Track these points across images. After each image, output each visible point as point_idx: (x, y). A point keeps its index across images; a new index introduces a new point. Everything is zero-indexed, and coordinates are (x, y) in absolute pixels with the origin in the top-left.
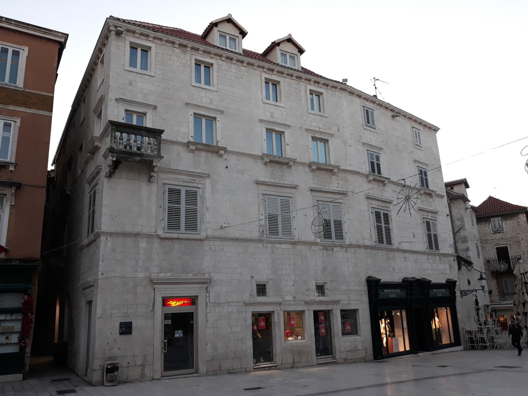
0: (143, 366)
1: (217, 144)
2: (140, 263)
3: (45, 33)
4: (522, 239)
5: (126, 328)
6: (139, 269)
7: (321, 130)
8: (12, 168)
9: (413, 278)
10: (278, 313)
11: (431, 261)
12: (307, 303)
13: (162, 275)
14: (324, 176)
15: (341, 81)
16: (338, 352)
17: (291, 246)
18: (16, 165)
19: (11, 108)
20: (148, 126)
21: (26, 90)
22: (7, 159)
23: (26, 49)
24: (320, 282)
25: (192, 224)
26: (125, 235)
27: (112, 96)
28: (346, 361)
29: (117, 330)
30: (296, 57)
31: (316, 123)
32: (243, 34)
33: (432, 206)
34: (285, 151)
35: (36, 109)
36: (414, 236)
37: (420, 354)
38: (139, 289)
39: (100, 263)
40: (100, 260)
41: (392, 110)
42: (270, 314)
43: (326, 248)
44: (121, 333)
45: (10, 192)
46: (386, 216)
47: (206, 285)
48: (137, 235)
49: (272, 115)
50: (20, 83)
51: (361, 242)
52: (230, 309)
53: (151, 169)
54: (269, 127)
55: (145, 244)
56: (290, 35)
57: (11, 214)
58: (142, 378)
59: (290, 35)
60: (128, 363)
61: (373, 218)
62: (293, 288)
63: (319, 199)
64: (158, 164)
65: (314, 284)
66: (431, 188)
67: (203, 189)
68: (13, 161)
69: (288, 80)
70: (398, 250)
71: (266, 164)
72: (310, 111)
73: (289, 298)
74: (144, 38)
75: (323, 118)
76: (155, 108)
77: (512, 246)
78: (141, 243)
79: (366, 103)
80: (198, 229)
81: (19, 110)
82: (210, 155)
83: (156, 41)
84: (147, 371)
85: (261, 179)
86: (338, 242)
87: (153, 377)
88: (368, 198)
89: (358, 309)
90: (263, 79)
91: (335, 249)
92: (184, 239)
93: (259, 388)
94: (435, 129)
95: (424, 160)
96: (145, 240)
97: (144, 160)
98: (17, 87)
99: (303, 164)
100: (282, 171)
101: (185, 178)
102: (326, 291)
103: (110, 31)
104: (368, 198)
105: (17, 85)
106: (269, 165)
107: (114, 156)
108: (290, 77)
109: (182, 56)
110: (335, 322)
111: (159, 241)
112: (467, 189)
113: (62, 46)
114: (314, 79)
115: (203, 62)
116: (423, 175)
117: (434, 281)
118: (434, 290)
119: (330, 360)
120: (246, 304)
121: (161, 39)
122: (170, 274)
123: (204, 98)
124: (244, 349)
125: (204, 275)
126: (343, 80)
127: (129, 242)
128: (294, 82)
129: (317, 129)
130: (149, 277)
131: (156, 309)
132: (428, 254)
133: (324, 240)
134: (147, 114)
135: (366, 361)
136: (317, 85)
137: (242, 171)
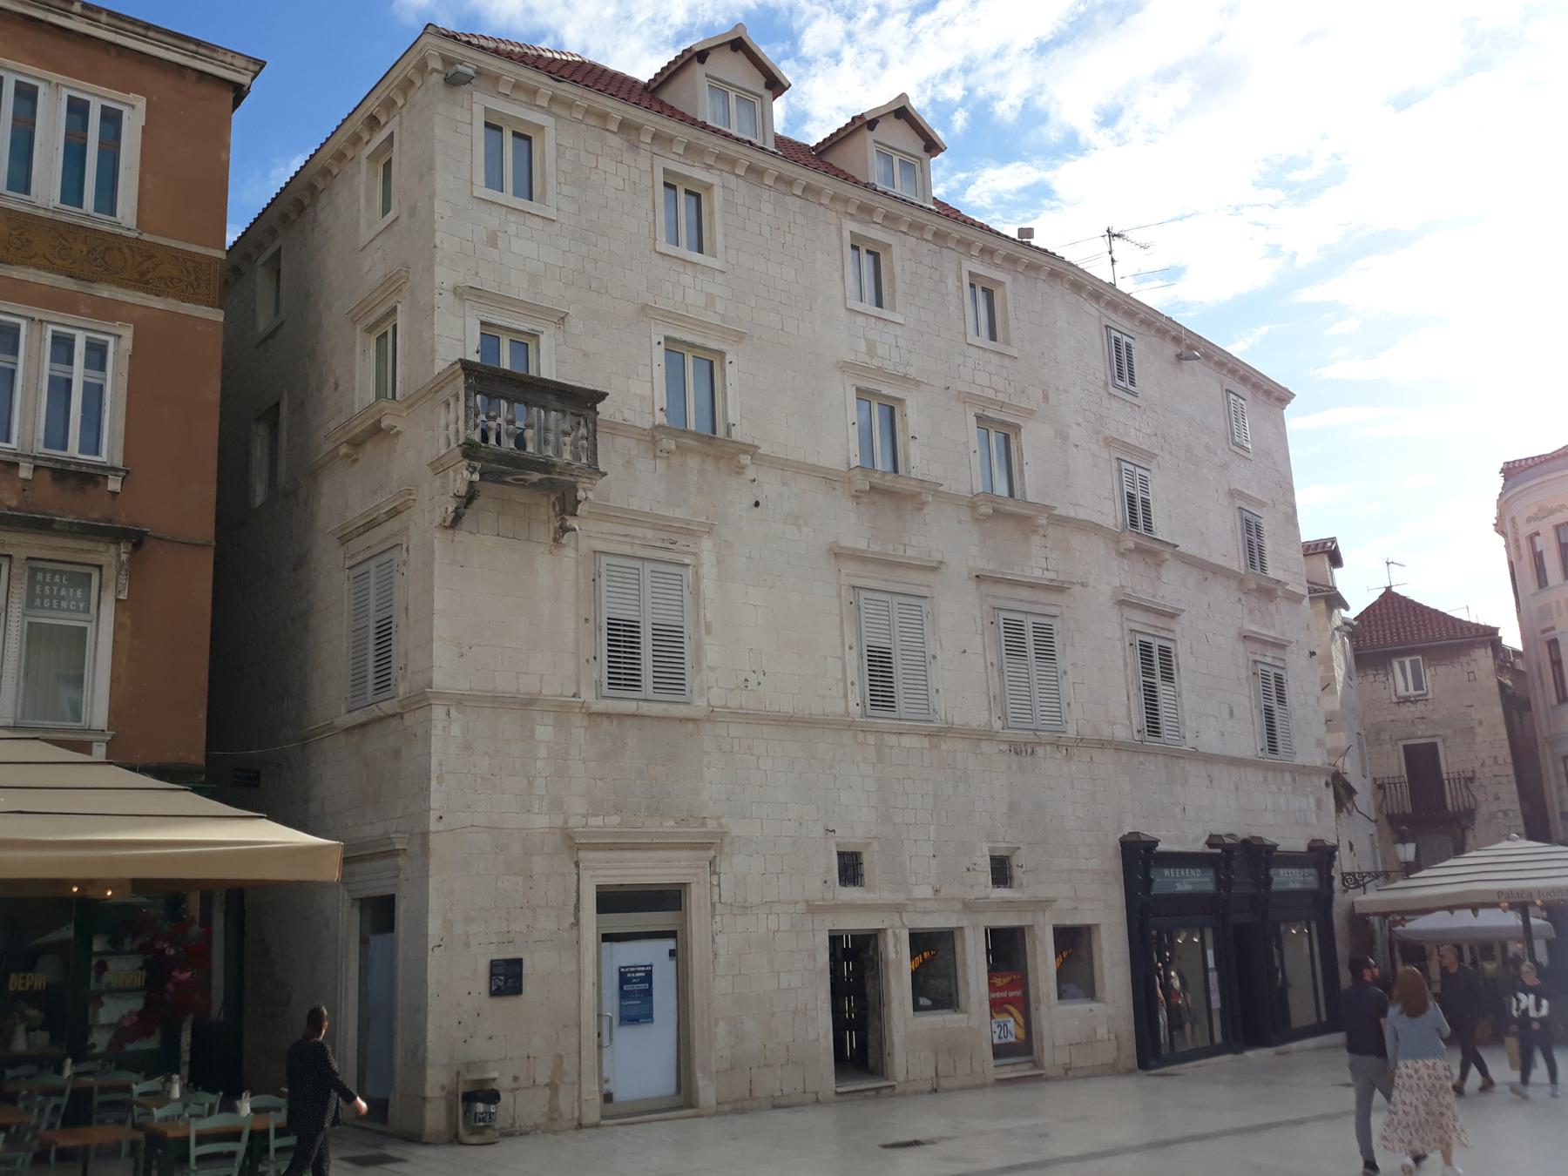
0: (553, 1086)
1: (728, 433)
2: (540, 783)
3: (194, 55)
4: (1480, 723)
5: (507, 978)
7: (1001, 397)
8: (114, 484)
9: (1230, 835)
10: (895, 935)
12: (968, 907)
13: (595, 821)
15: (1015, 235)
16: (1047, 1045)
17: (926, 742)
19: (106, 294)
20: (545, 375)
21: (146, 237)
22: (97, 453)
23: (141, 103)
24: (1002, 848)
26: (498, 702)
27: (444, 276)
28: (1068, 1073)
29: (482, 983)
30: (917, 166)
32: (776, 86)
34: (907, 459)
35: (175, 297)
37: (1250, 1054)
39: (433, 783)
40: (434, 776)
41: (1177, 340)
44: (496, 992)
45: (111, 556)
46: (1165, 652)
47: (712, 853)
48: (526, 704)
49: (871, 348)
51: (1106, 732)
53: (569, 509)
54: (864, 384)
55: (550, 729)
56: (903, 96)
57: (118, 627)
58: (551, 1125)
59: (903, 96)
60: (516, 1079)
61: (1135, 659)
62: (933, 862)
63: (857, 582)
64: (590, 495)
67: (697, 567)
68: (118, 463)
70: (1195, 755)
71: (979, 520)
72: (663, 246)
75: (1007, 362)
81: (128, 299)
83: (556, 109)
84: (565, 1102)
85: (847, 542)
87: (580, 1118)
88: (1122, 603)
89: (1097, 925)
90: (847, 235)
91: (1040, 751)
92: (651, 717)
93: (916, 1143)
94: (1282, 397)
98: (119, 225)
99: (954, 499)
101: (650, 534)
102: (1017, 873)
103: (422, 68)
105: (119, 218)
108: (917, 234)
110: (1039, 959)
112: (1336, 571)
113: (239, 93)
114: (981, 240)
116: (1252, 531)
118: (1166, 872)
119: (1025, 1070)
120: (813, 909)
121: (570, 105)
122: (616, 819)
123: (695, 293)
125: (704, 825)
126: (1021, 231)
129: (989, 393)
130: (563, 829)
131: (583, 920)
132: (1267, 768)
133: (869, 712)
134: (542, 338)
136: (987, 258)
137: (797, 518)
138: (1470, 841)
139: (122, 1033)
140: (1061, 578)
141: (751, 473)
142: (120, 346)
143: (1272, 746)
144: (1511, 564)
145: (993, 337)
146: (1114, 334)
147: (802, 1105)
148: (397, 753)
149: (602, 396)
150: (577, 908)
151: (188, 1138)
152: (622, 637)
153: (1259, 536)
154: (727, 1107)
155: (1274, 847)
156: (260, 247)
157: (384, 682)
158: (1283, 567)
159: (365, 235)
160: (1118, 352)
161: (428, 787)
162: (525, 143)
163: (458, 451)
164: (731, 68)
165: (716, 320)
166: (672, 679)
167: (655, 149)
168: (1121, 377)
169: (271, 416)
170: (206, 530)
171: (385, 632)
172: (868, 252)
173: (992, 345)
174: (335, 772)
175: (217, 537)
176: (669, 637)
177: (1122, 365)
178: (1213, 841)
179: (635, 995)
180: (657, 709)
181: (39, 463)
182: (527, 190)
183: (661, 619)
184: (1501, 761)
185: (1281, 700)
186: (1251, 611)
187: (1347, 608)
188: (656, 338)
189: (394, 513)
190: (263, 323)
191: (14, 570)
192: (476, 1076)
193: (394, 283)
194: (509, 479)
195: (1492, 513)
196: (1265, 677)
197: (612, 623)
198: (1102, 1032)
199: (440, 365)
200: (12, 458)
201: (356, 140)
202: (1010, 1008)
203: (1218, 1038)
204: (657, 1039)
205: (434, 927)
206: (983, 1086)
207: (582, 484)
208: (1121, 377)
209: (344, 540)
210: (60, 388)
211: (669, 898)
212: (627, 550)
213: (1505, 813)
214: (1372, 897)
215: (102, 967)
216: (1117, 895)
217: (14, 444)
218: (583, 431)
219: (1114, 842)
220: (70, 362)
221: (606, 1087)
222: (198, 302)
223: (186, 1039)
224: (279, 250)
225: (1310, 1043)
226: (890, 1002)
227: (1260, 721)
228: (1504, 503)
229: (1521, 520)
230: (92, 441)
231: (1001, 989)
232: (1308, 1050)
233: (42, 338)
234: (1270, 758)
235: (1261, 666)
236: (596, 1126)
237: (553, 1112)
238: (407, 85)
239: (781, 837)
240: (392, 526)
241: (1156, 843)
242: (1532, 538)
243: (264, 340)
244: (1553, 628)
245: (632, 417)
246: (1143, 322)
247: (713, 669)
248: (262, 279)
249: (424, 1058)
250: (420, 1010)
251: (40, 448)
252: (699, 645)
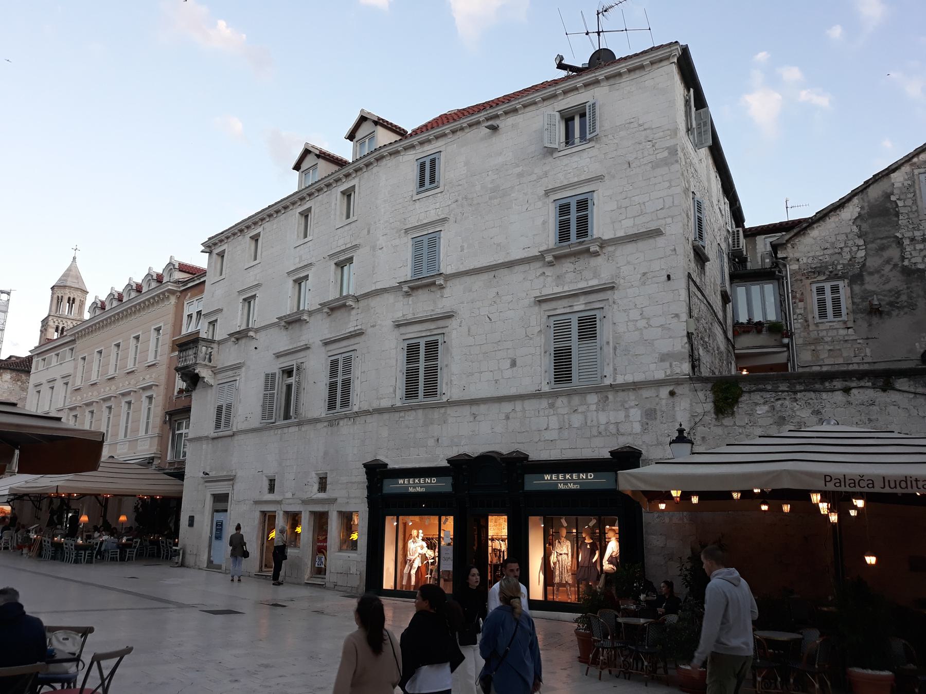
12: (305, 502)
14: (423, 295)
17: (296, 429)
25: (432, 389)
28: (335, 587)
54: (294, 278)
61: (402, 356)
70: (451, 404)
73: (289, 495)
88: (398, 326)
117: (537, 454)
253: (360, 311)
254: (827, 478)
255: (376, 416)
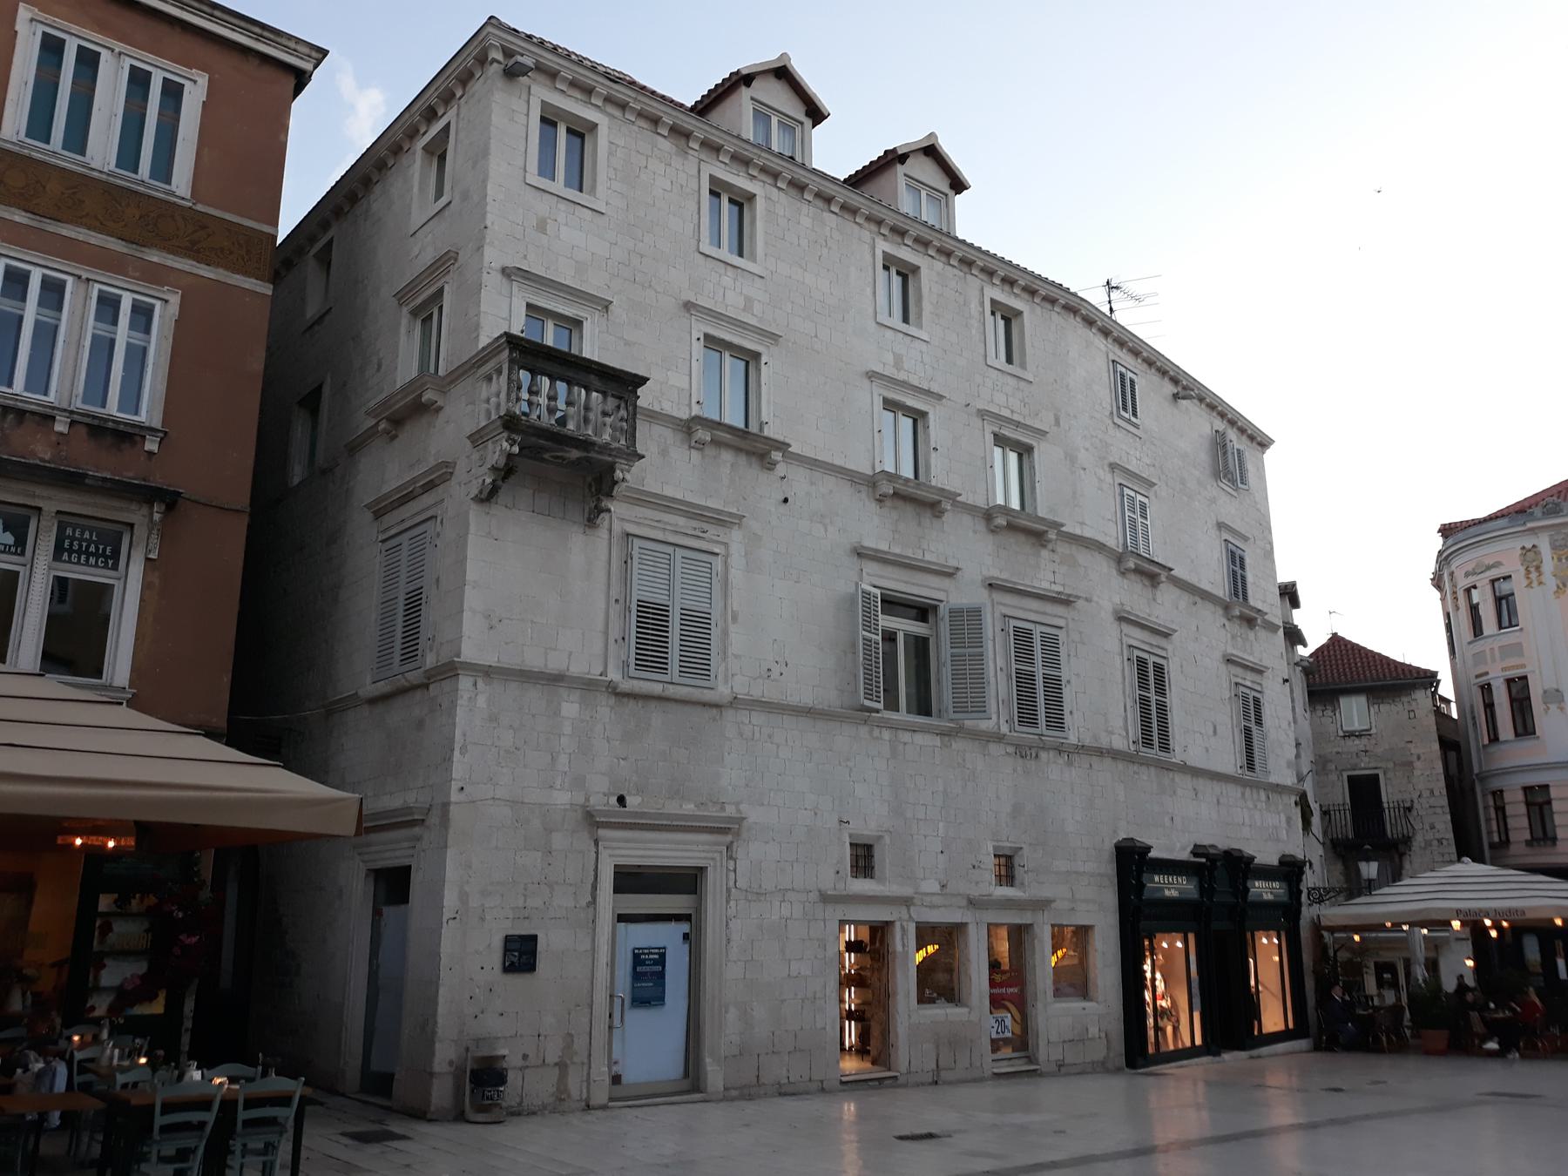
0: (562, 1066)
1: (761, 429)
2: (563, 759)
5: (521, 954)
6: (558, 782)
7: (1016, 417)
8: (151, 445)
9: (1212, 846)
11: (1250, 804)
12: (973, 903)
14: (1019, 546)
16: (1042, 1043)
17: (937, 741)
18: (164, 437)
19: (155, 259)
20: (586, 354)
21: (199, 207)
23: (203, 80)
27: (494, 256)
28: (1061, 1069)
31: (1003, 397)
33: (1251, 654)
35: (226, 268)
36: (1215, 732)
38: (558, 841)
39: (457, 753)
41: (1175, 381)
42: (882, 928)
43: (1023, 751)
44: (509, 968)
46: (1159, 669)
47: (729, 838)
48: (555, 680)
50: (182, 181)
51: (1104, 742)
52: (786, 912)
54: (891, 395)
57: (146, 586)
58: (558, 1105)
60: (525, 1057)
61: (1132, 674)
64: (628, 477)
65: (991, 850)
66: (1252, 602)
67: (727, 557)
68: (157, 423)
69: (939, 265)
70: (1185, 769)
74: (578, 95)
75: (1022, 384)
76: (606, 306)
77: (1390, 775)
78: (564, 704)
79: (1119, 352)
80: (712, 674)
82: (742, 460)
84: (574, 1084)
85: (869, 543)
86: (1052, 736)
91: (1043, 755)
92: (676, 701)
93: (930, 1136)
94: (1263, 443)
95: (1237, 525)
96: (576, 695)
97: (588, 460)
98: (173, 194)
99: (971, 509)
100: (919, 524)
101: (681, 521)
104: (1122, 618)
105: (173, 187)
106: (888, 503)
107: (515, 441)
108: (943, 259)
109: (677, 162)
111: (612, 700)
113: (301, 79)
115: (728, 187)
116: (1236, 561)
123: (728, 294)
124: (819, 1026)
125: (723, 809)
127: (534, 696)
128: (953, 273)
129: (1006, 413)
130: (584, 806)
133: (1017, 728)
135: (1107, 1071)
136: (1007, 288)
138: (1407, 865)
139: (124, 997)
140: (1068, 591)
141: (781, 469)
142: (165, 313)
143: (1251, 766)
144: (1447, 616)
145: (1009, 360)
146: (1120, 368)
147: (807, 1093)
148: (420, 724)
149: (643, 380)
150: (594, 887)
151: (153, 1106)
152: (652, 619)
153: (1243, 567)
154: (734, 1093)
155: (1253, 858)
156: (313, 240)
157: (411, 651)
158: (1262, 598)
159: (417, 219)
160: (1123, 385)
161: (450, 759)
162: (578, 141)
163: (499, 423)
164: (775, 95)
165: (753, 322)
166: (698, 663)
167: (703, 157)
168: (1125, 409)
169: (312, 402)
170: (243, 500)
171: (414, 604)
172: (898, 273)
173: (1009, 368)
174: (359, 741)
175: (251, 505)
176: (698, 623)
177: (1126, 397)
178: (1198, 851)
179: (647, 979)
180: (681, 692)
181: (76, 417)
182: (578, 180)
183: (689, 604)
184: (1437, 793)
185: (1259, 722)
186: (1233, 637)
187: (1305, 645)
188: (695, 335)
189: (430, 486)
190: (311, 311)
191: (43, 522)
192: (485, 1052)
193: (445, 262)
194: (546, 456)
195: (1431, 566)
196: (1245, 699)
197: (642, 605)
198: (1094, 1031)
199: (484, 341)
200: (49, 411)
201: (413, 134)
202: (1008, 1004)
203: (1198, 1041)
204: (671, 1016)
205: (450, 899)
206: (981, 1080)
207: (621, 464)
208: (1125, 409)
209: (378, 515)
210: (103, 347)
211: (688, 881)
212: (660, 536)
213: (1440, 841)
214: (1335, 913)
215: (107, 929)
216: (1111, 898)
217: (52, 398)
218: (623, 413)
219: (1109, 846)
220: (115, 322)
221: (615, 1068)
222: (246, 273)
223: (189, 1006)
224: (330, 242)
225: (1280, 1047)
226: (895, 993)
227: (1240, 739)
228: (1443, 559)
229: (1459, 574)
230: (131, 396)
231: (1001, 985)
232: (1276, 1055)
233: (87, 298)
234: (1248, 775)
235: (1242, 689)
236: (604, 1107)
237: (561, 1095)
238: (466, 78)
239: (810, 811)
240: (427, 499)
241: (1149, 848)
242: (1468, 591)
243: (311, 327)
244: (1487, 673)
245: (668, 408)
246: (1146, 360)
247: (736, 656)
248: (310, 265)
249: (434, 1033)
250: (434, 983)
251: (78, 404)
252: (725, 633)
253: (1056, 558)
254: (1509, 910)
255: (1108, 761)
